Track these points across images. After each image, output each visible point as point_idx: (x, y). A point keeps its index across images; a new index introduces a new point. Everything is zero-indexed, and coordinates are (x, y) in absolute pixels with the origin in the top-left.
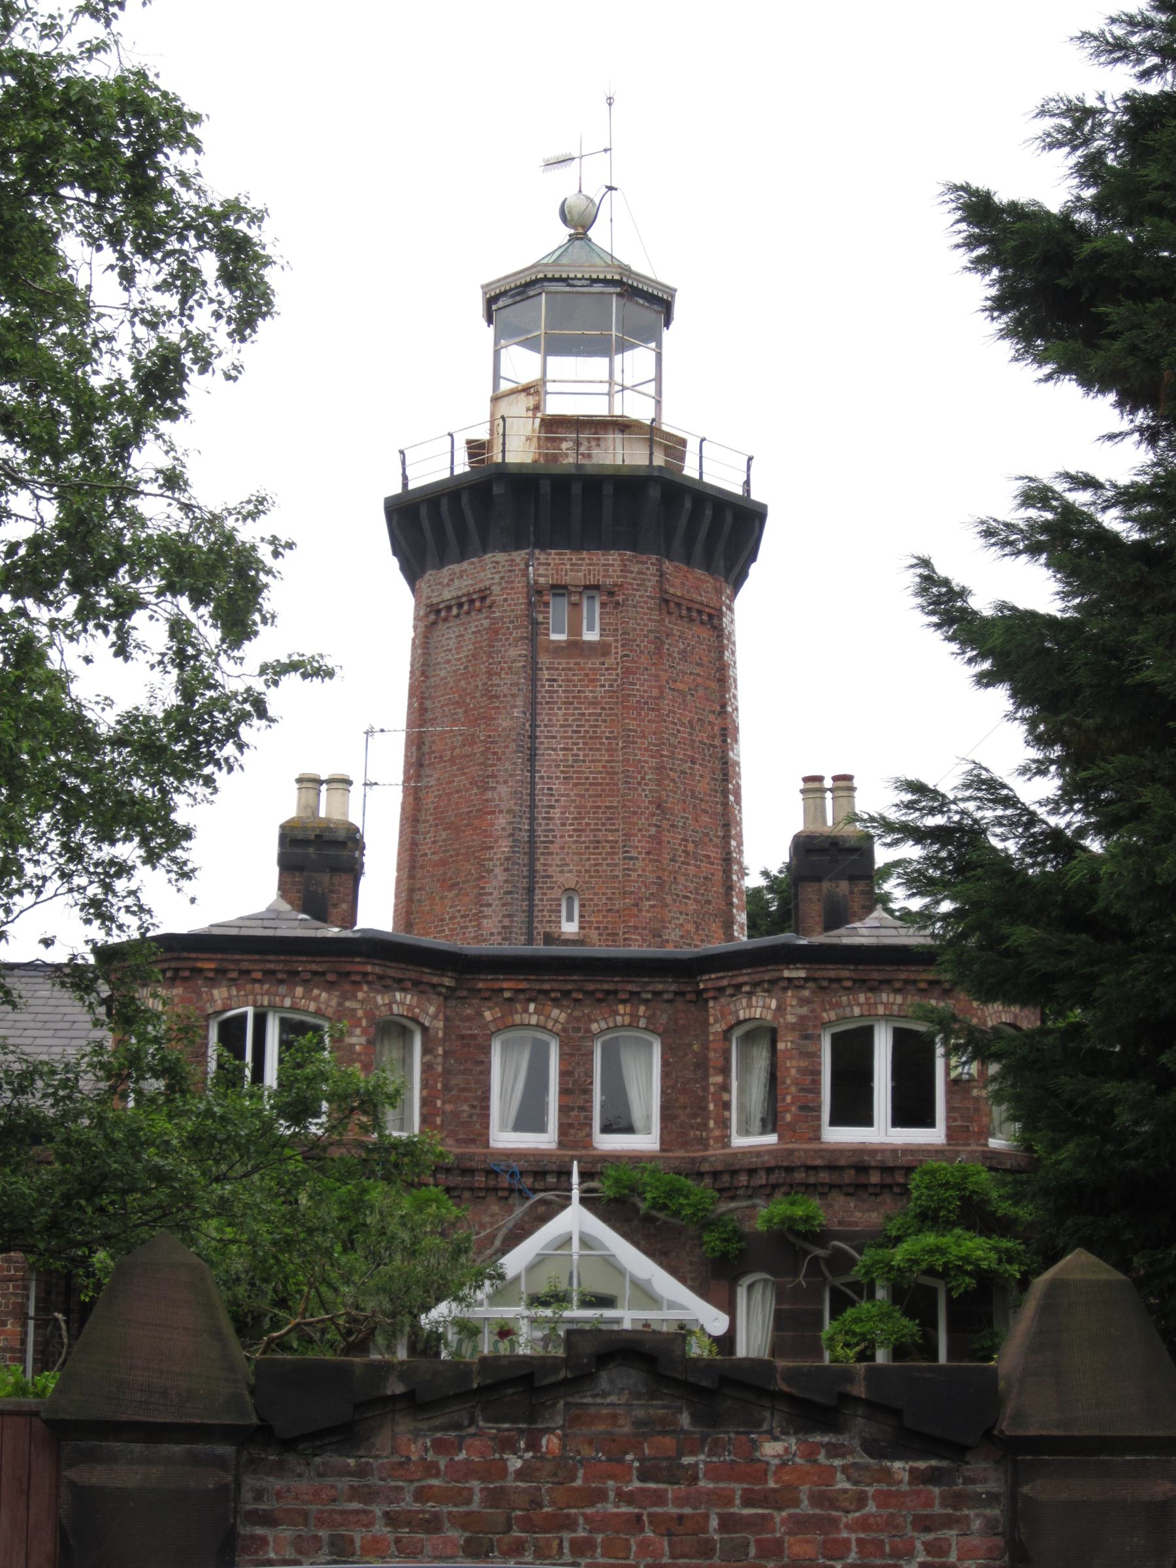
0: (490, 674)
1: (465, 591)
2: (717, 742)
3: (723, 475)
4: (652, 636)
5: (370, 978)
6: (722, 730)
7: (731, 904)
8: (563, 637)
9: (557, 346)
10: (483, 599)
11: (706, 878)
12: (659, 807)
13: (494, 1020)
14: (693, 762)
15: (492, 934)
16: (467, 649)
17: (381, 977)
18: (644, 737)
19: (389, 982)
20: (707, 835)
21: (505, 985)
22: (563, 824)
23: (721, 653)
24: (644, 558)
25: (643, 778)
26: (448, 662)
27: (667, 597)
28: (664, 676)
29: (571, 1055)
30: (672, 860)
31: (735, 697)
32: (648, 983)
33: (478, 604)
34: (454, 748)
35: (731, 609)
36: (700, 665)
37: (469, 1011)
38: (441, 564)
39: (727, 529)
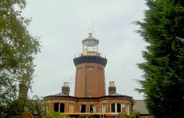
3: (103, 56)
6: (104, 79)
9: (89, 46)
17: (70, 99)
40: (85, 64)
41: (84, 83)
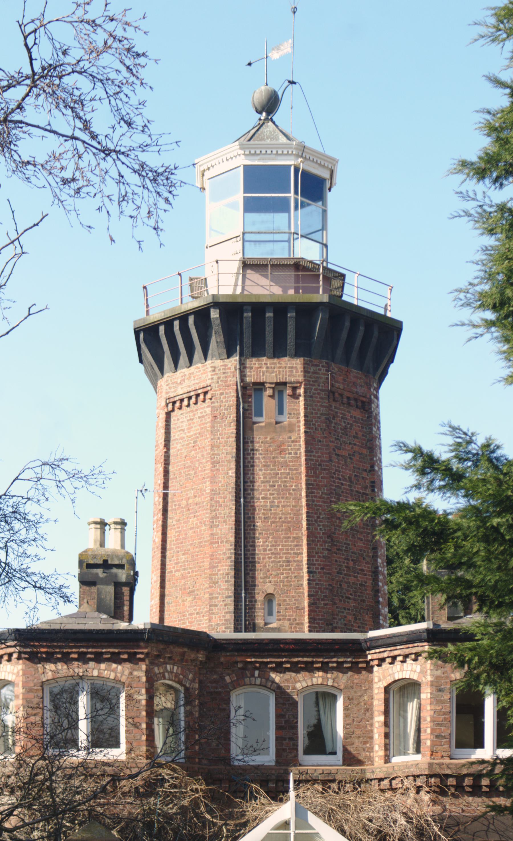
1: (193, 388)
2: (368, 491)
4: (323, 418)
7: (378, 602)
10: (205, 393)
11: (361, 585)
13: (232, 682)
15: (218, 625)
16: (196, 429)
18: (319, 488)
20: (362, 555)
21: (239, 659)
29: (284, 704)
30: (338, 573)
34: (189, 498)
35: (377, 398)
37: (215, 677)
39: (374, 340)
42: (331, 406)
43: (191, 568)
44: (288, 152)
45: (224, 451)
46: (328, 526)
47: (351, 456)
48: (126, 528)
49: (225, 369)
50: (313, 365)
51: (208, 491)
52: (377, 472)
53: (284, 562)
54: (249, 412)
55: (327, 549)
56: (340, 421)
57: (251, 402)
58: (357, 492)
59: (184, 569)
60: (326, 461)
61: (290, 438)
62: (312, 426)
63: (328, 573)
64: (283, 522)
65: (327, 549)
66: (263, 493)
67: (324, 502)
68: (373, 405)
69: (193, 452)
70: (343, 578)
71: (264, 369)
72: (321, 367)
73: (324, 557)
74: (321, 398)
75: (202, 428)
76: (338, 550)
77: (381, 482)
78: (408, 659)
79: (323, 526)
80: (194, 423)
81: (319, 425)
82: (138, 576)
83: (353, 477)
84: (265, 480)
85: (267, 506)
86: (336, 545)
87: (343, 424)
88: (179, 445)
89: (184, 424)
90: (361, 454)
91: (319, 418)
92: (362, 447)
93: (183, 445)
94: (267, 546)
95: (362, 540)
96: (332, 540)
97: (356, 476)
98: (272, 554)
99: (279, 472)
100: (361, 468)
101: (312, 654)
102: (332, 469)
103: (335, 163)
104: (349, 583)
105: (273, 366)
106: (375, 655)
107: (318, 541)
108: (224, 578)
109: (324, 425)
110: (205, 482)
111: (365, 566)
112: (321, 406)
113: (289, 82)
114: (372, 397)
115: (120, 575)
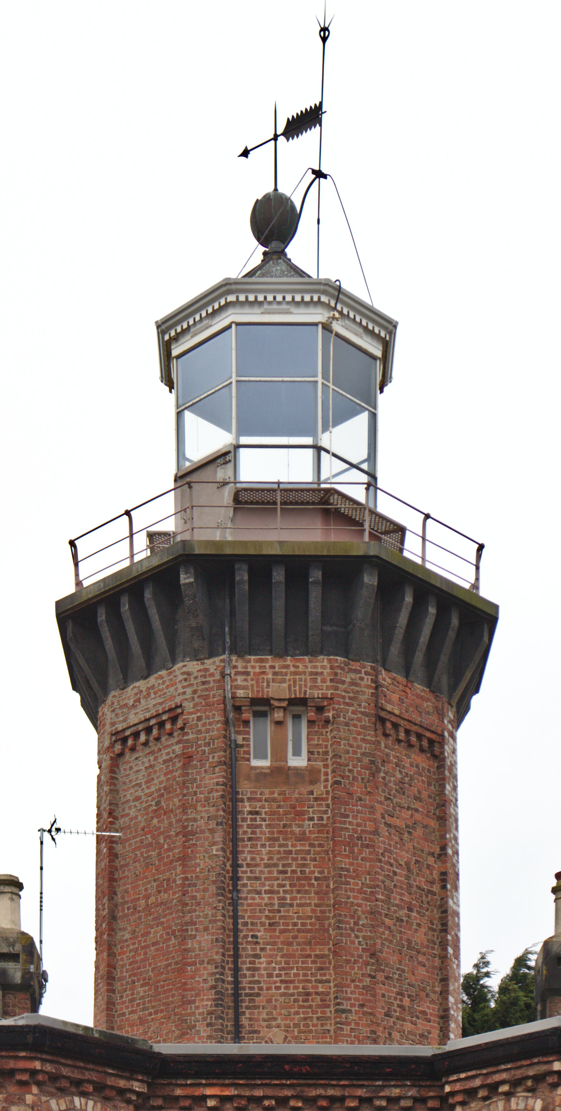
0: (184, 808)
1: (153, 712)
2: (436, 888)
3: (447, 562)
4: (366, 760)
5: (40, 1077)
8: (265, 763)
10: (174, 720)
12: (373, 955)
14: (410, 909)
16: (159, 780)
17: (54, 1078)
18: (357, 877)
19: (64, 1084)
20: (424, 989)
21: (208, 1092)
22: (270, 975)
23: (443, 787)
24: (355, 666)
25: (356, 924)
26: (137, 799)
27: (383, 714)
28: (380, 809)
31: (456, 839)
32: (383, 1087)
33: (168, 726)
34: (147, 897)
35: (454, 738)
36: (417, 799)
38: (126, 681)
40: (213, 664)
41: (244, 828)
42: (379, 743)
43: (153, 1007)
44: (312, 298)
45: (204, 814)
46: (371, 938)
47: (411, 828)
48: (21, 893)
49: (205, 676)
50: (351, 670)
51: (179, 882)
52: (452, 857)
53: (299, 994)
54: (245, 749)
55: (370, 976)
56: (394, 770)
57: (248, 733)
58: (418, 887)
59: (144, 1009)
60: (371, 833)
61: (312, 793)
62: (347, 773)
63: (371, 1014)
64: (299, 931)
65: (370, 976)
66: (267, 883)
67: (364, 899)
68: (446, 747)
69: (155, 821)
70: (394, 1023)
71: (270, 676)
72: (363, 675)
73: (364, 987)
74: (364, 727)
75: (168, 780)
76: (387, 978)
77: (457, 875)
78: (519, 1089)
79: (364, 937)
80: (155, 772)
81: (359, 773)
82: (46, 981)
83: (413, 863)
84: (271, 862)
85: (274, 904)
86: (383, 971)
87: (399, 776)
88: (133, 810)
89: (140, 776)
90: (425, 827)
91: (359, 760)
92: (427, 816)
93: (140, 810)
94: (274, 969)
95: (424, 966)
96: (377, 961)
97: (417, 862)
98: (282, 981)
99: (293, 849)
100: (426, 849)
101: (342, 1083)
102: (379, 847)
103: (391, 327)
104: (404, 1032)
105: (284, 670)
106: (458, 1084)
107: (355, 962)
108: (205, 1019)
109: (367, 772)
110: (175, 868)
111: (428, 1007)
112: (363, 740)
113: (314, 172)
114: (446, 734)
115: (11, 972)
